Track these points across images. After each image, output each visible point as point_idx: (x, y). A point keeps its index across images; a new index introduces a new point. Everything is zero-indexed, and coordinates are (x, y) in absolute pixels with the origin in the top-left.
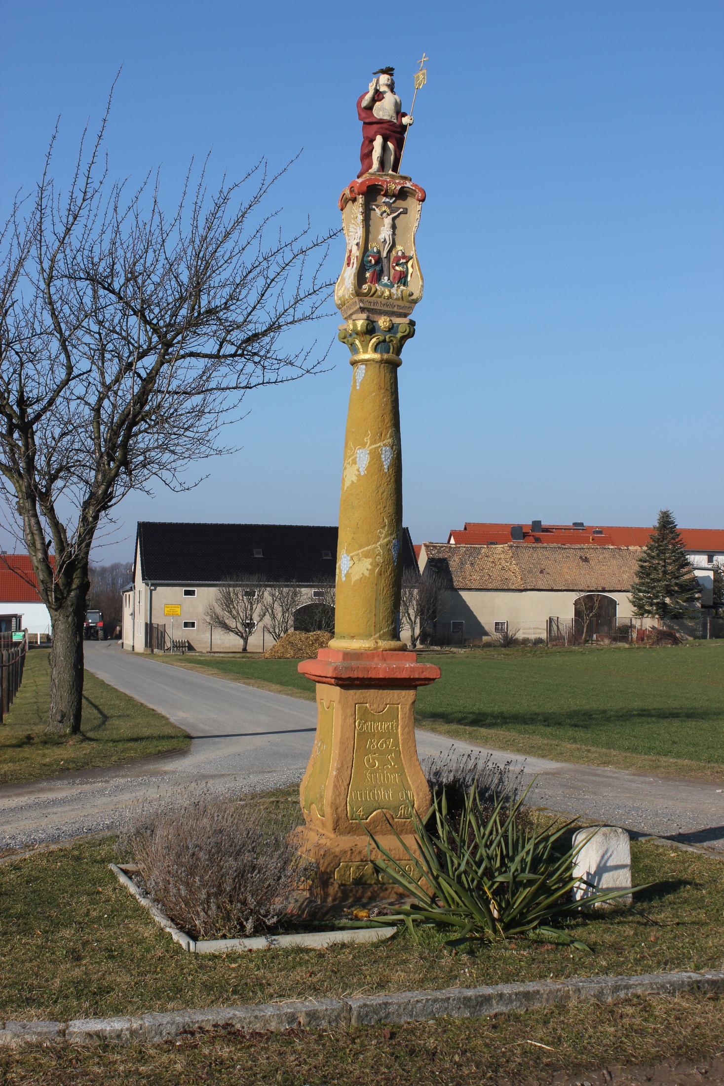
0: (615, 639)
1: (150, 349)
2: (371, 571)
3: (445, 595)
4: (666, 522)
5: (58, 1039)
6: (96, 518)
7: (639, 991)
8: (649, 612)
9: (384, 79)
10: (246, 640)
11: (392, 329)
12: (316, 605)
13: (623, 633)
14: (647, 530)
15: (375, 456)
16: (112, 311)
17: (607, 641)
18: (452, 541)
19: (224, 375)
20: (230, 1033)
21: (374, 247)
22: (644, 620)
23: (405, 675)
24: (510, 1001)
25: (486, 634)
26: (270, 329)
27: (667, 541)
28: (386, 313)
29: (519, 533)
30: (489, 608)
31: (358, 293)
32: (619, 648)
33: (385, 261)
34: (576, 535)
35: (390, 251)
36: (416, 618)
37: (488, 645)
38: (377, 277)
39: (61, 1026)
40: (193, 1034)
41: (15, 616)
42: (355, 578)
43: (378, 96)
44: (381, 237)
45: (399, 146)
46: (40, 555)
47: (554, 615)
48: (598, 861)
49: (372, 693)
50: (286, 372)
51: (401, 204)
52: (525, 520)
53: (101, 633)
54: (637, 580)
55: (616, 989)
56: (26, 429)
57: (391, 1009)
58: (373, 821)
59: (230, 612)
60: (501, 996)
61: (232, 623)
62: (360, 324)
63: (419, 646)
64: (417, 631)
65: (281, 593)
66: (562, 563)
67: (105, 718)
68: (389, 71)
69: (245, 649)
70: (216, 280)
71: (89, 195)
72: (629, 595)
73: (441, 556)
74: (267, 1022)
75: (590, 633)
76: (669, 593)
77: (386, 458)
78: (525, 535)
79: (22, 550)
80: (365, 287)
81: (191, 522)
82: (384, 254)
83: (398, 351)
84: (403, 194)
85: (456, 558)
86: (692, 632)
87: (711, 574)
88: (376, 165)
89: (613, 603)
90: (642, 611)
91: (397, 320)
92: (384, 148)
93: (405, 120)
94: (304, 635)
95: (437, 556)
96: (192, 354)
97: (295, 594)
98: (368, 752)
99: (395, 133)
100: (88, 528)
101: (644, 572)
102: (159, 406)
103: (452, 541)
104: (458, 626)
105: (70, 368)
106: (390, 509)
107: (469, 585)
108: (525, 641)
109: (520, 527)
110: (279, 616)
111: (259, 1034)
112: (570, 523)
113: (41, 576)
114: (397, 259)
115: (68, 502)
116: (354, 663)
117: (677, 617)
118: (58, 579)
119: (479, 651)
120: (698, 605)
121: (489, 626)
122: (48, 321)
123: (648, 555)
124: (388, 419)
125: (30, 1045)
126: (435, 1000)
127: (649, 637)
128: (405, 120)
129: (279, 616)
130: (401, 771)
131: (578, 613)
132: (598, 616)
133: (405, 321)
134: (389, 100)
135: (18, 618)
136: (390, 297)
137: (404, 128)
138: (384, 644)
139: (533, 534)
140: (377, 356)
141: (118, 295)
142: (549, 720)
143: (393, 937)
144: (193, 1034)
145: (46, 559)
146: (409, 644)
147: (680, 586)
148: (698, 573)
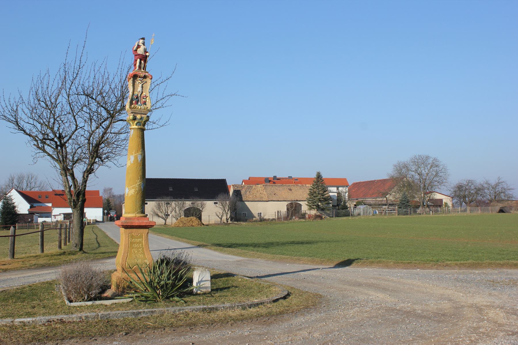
0: (300, 218)
1: (108, 118)
2: (134, 193)
3: (239, 204)
4: (319, 176)
5: (11, 323)
6: (87, 176)
7: (187, 311)
8: (313, 208)
9: (141, 41)
10: (166, 220)
11: (141, 118)
12: (191, 208)
13: (303, 216)
14: (312, 178)
15: (136, 158)
16: (94, 106)
17: (297, 219)
20: (62, 321)
21: (136, 93)
22: (311, 211)
23: (144, 224)
24: (147, 313)
25: (255, 217)
27: (320, 182)
28: (140, 114)
29: (268, 181)
30: (255, 208)
31: (130, 108)
32: (301, 222)
33: (139, 98)
35: (141, 95)
36: (228, 210)
37: (256, 221)
38: (137, 103)
39: (13, 320)
40: (51, 322)
42: (129, 195)
43: (139, 46)
44: (138, 90)
45: (145, 62)
46: (68, 190)
48: (200, 279)
49: (134, 230)
50: (155, 126)
51: (144, 80)
52: (270, 175)
53: (115, 219)
54: (309, 197)
55: (180, 310)
56: (63, 145)
57: (111, 315)
58: (135, 269)
59: (160, 210)
60: (144, 312)
61: (160, 214)
62: (131, 117)
63: (229, 221)
64: (228, 216)
66: (282, 191)
67: (99, 246)
68: (143, 39)
71: (81, 67)
72: (306, 202)
73: (238, 189)
74: (73, 319)
75: (292, 216)
76: (320, 201)
77: (140, 158)
78: (270, 181)
79: (61, 188)
80: (133, 106)
81: (208, 178)
82: (139, 96)
83: (144, 125)
84: (145, 77)
85: (244, 190)
86: (328, 215)
87: (336, 194)
88: (137, 68)
89: (300, 205)
90: (311, 208)
91: (143, 116)
92: (140, 63)
93: (147, 54)
94: (186, 218)
95: (237, 189)
96: (121, 120)
97: (183, 203)
98: (133, 248)
99: (144, 58)
100: (85, 181)
101: (311, 194)
102: (107, 138)
105: (77, 126)
106: (141, 174)
107: (248, 199)
108: (269, 220)
109: (268, 178)
110: (178, 211)
111: (71, 322)
112: (287, 177)
113: (69, 197)
114: (143, 97)
115: (79, 170)
116: (128, 221)
117: (323, 210)
118: (75, 198)
119: (251, 223)
120: (331, 205)
121: (256, 215)
122: (68, 108)
124: (140, 146)
125: (3, 325)
126: (124, 313)
128: (147, 54)
129: (178, 211)
130: (144, 254)
131: (288, 209)
132: (295, 210)
133: (146, 116)
136: (141, 109)
137: (146, 56)
138: (138, 215)
139: (273, 181)
140: (137, 127)
141: (95, 100)
142: (255, 246)
143: (131, 301)
144: (51, 322)
145: (70, 191)
146: (225, 221)
147: (324, 199)
148: (331, 194)
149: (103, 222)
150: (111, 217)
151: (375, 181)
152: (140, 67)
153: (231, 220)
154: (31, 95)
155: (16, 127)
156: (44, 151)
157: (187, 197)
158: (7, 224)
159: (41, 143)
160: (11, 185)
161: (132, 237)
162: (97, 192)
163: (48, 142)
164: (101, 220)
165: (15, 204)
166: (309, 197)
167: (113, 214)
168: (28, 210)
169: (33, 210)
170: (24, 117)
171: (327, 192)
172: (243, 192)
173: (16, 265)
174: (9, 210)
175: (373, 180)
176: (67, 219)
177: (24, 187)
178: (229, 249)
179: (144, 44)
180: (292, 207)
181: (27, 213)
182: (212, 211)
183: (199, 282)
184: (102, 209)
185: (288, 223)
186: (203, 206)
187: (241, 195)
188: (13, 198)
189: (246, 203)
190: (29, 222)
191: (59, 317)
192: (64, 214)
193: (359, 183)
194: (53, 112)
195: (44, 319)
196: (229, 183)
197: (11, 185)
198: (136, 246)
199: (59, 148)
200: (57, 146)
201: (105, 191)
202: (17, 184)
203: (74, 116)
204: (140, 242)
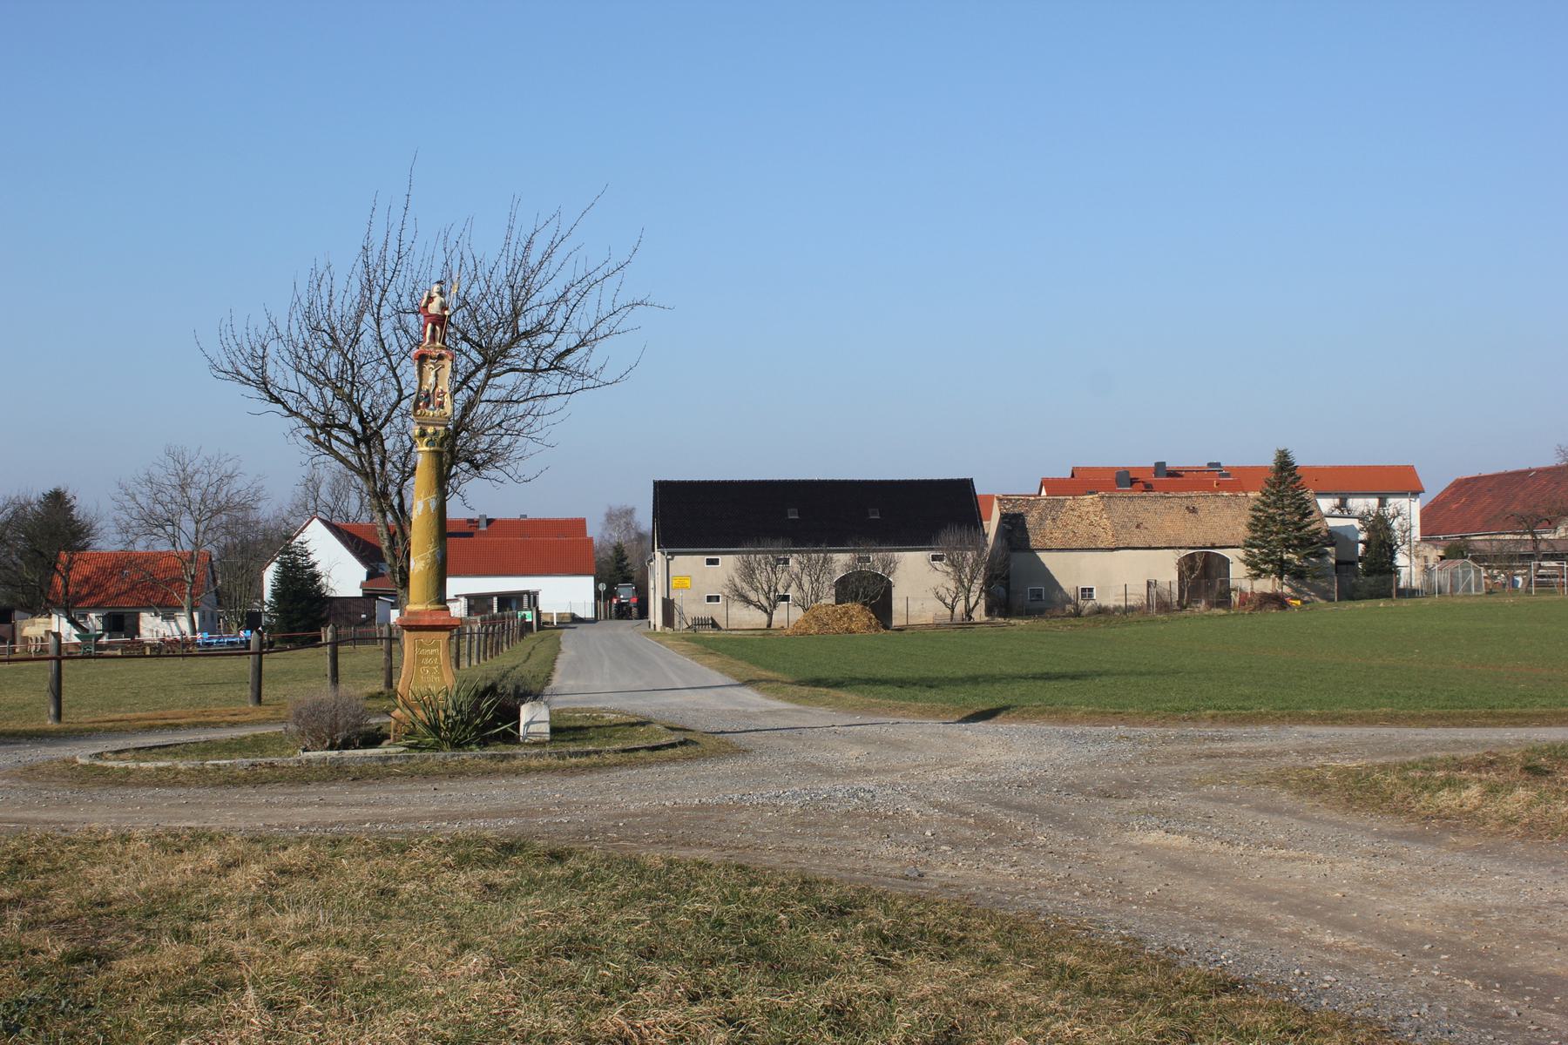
4: (1284, 464)
10: (770, 615)
11: (436, 433)
15: (427, 504)
18: (1044, 493)
19: (545, 384)
21: (425, 387)
26: (582, 343)
30: (1069, 570)
34: (1165, 479)
38: (427, 405)
41: (527, 593)
43: (430, 299)
47: (1152, 578)
49: (425, 633)
52: (1140, 458)
53: (634, 610)
54: (1249, 534)
61: (753, 596)
62: (417, 432)
65: (809, 560)
69: (769, 625)
70: (534, 301)
72: (1241, 553)
73: (1016, 511)
78: (1133, 482)
81: (696, 479)
89: (1225, 562)
92: (434, 330)
95: (1011, 511)
101: (1257, 524)
103: (1044, 493)
104: (1037, 595)
105: (400, 391)
110: (806, 586)
123: (1264, 503)
127: (1250, 601)
134: (438, 300)
135: (533, 597)
142: (902, 683)
147: (1301, 539)
149: (595, 620)
150: (620, 605)
151: (1530, 471)
152: (433, 338)
153: (989, 611)
154: (294, 321)
155: (264, 395)
156: (330, 449)
157: (838, 540)
158: (293, 630)
159: (323, 428)
160: (311, 504)
161: (421, 646)
162: (579, 525)
163: (335, 432)
164: (590, 614)
165: (318, 568)
166: (1249, 534)
167: (625, 594)
168: (363, 585)
169: (378, 586)
170: (283, 376)
171: (1311, 518)
172: (1031, 520)
173: (260, 716)
174: (301, 587)
175: (1525, 467)
176: (477, 614)
177: (353, 511)
178: (832, 691)
179: (441, 293)
180: (1192, 569)
181: (359, 593)
182: (921, 583)
183: (528, 725)
184: (592, 579)
185: (1164, 622)
186: (886, 564)
187: (1025, 530)
188: (310, 547)
189: (1042, 556)
190: (363, 623)
191: (269, 760)
192: (468, 597)
193: (1475, 479)
194: (350, 356)
195: (246, 762)
196: (980, 490)
197: (311, 504)
198: (427, 661)
199: (362, 446)
200: (357, 442)
201: (611, 517)
202: (330, 500)
203: (394, 370)
204: (434, 656)
